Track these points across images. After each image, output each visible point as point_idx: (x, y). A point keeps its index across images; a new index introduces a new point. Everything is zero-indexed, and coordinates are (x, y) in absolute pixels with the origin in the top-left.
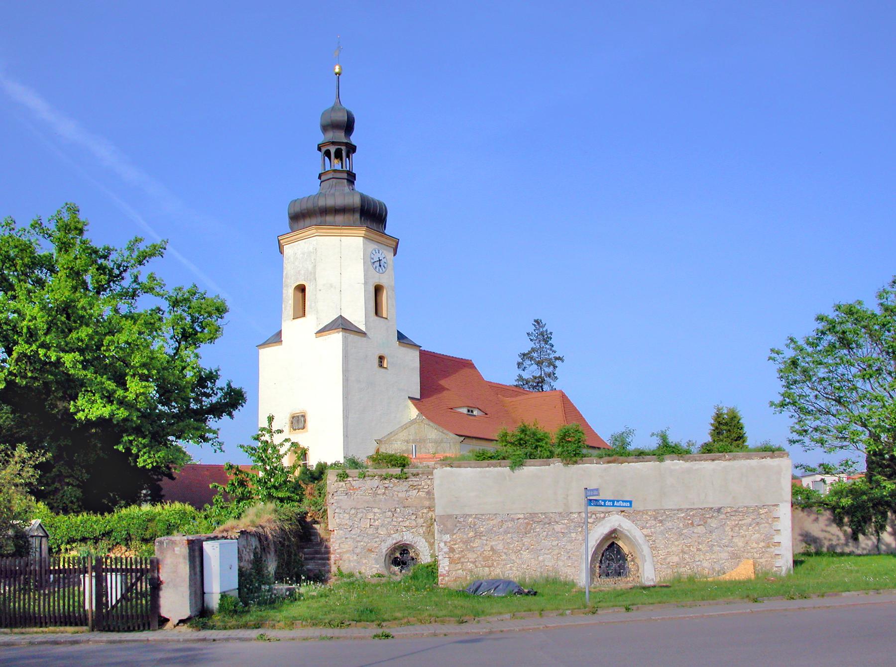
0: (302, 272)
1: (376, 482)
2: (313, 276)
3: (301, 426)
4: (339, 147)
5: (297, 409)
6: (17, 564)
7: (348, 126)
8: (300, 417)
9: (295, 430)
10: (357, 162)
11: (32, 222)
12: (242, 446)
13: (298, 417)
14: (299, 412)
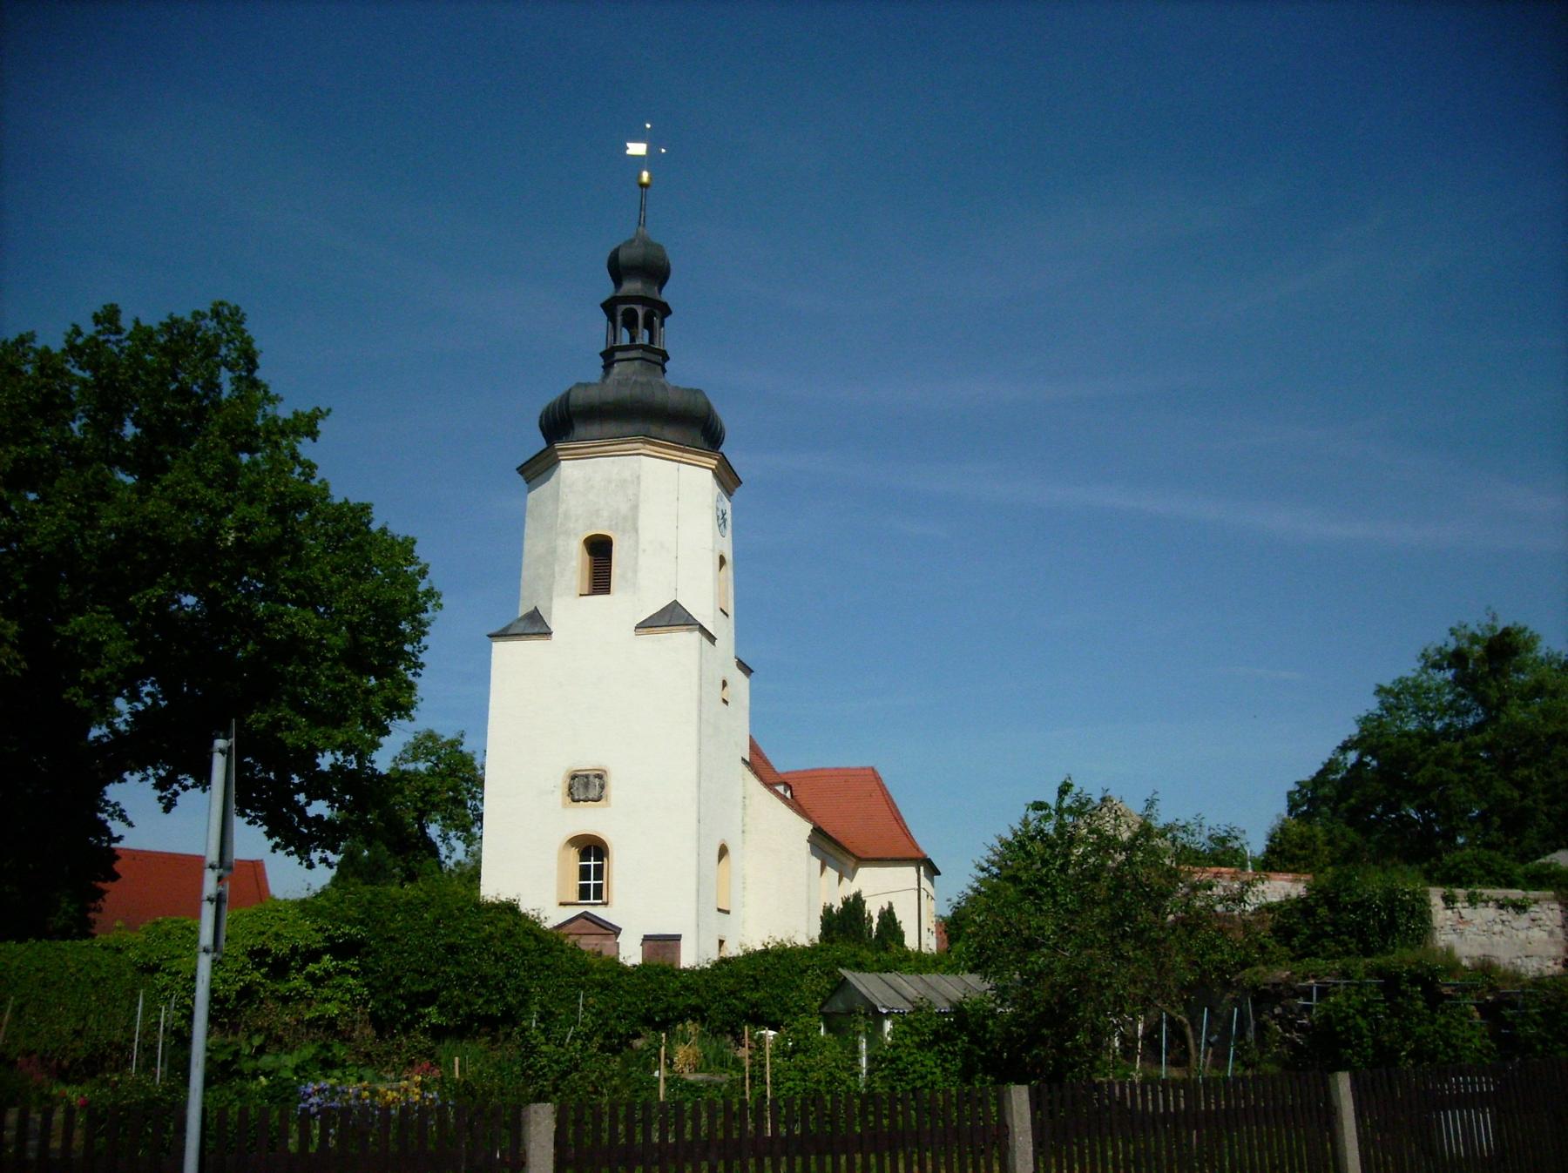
0: (605, 514)
1: (1491, 912)
2: (631, 522)
3: (593, 793)
4: (628, 306)
5: (586, 763)
6: (227, 874)
7: (657, 272)
8: (591, 778)
9: (578, 801)
10: (671, 336)
11: (1455, 625)
13: (587, 777)
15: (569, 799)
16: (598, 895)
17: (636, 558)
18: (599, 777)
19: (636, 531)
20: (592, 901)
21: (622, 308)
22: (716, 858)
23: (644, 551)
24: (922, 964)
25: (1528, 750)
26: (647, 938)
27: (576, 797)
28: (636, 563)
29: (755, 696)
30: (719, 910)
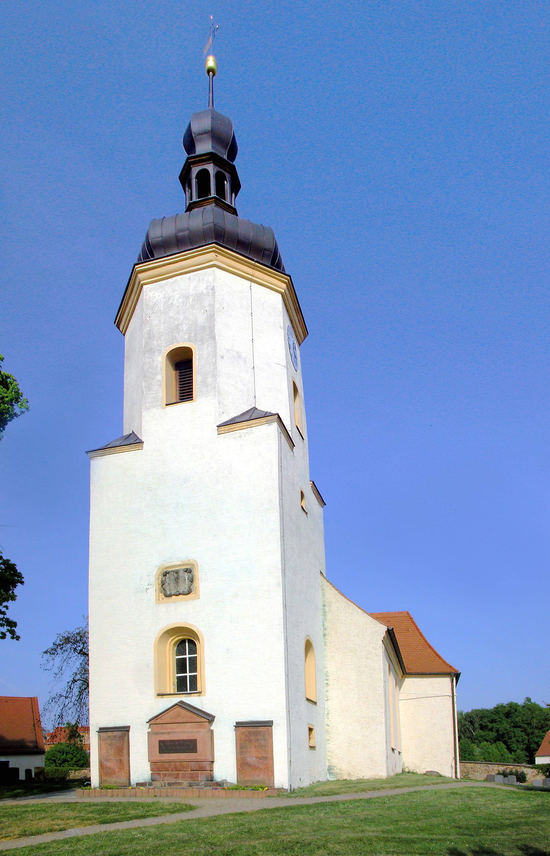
3: (183, 587)
8: (181, 573)
9: (170, 596)
12: (46, 652)
13: (177, 572)
14: (178, 563)
15: (162, 596)
16: (194, 686)
17: (215, 363)
18: (188, 571)
19: (214, 338)
20: (188, 691)
21: (195, 170)
22: (303, 655)
23: (222, 357)
24: (265, 818)
25: (194, 849)
26: (239, 725)
27: (168, 593)
28: (216, 368)
29: (326, 520)
30: (308, 700)
